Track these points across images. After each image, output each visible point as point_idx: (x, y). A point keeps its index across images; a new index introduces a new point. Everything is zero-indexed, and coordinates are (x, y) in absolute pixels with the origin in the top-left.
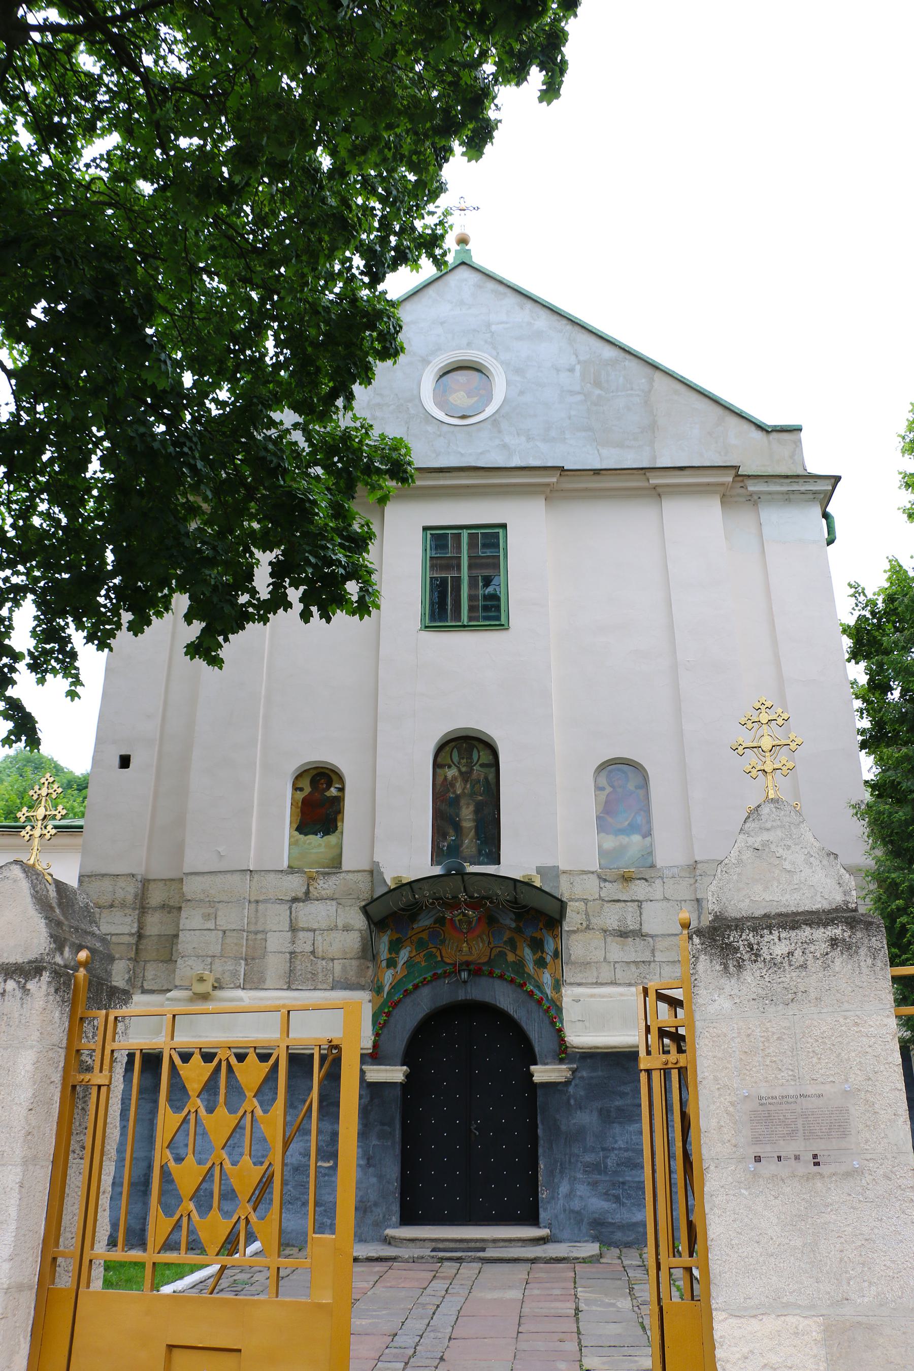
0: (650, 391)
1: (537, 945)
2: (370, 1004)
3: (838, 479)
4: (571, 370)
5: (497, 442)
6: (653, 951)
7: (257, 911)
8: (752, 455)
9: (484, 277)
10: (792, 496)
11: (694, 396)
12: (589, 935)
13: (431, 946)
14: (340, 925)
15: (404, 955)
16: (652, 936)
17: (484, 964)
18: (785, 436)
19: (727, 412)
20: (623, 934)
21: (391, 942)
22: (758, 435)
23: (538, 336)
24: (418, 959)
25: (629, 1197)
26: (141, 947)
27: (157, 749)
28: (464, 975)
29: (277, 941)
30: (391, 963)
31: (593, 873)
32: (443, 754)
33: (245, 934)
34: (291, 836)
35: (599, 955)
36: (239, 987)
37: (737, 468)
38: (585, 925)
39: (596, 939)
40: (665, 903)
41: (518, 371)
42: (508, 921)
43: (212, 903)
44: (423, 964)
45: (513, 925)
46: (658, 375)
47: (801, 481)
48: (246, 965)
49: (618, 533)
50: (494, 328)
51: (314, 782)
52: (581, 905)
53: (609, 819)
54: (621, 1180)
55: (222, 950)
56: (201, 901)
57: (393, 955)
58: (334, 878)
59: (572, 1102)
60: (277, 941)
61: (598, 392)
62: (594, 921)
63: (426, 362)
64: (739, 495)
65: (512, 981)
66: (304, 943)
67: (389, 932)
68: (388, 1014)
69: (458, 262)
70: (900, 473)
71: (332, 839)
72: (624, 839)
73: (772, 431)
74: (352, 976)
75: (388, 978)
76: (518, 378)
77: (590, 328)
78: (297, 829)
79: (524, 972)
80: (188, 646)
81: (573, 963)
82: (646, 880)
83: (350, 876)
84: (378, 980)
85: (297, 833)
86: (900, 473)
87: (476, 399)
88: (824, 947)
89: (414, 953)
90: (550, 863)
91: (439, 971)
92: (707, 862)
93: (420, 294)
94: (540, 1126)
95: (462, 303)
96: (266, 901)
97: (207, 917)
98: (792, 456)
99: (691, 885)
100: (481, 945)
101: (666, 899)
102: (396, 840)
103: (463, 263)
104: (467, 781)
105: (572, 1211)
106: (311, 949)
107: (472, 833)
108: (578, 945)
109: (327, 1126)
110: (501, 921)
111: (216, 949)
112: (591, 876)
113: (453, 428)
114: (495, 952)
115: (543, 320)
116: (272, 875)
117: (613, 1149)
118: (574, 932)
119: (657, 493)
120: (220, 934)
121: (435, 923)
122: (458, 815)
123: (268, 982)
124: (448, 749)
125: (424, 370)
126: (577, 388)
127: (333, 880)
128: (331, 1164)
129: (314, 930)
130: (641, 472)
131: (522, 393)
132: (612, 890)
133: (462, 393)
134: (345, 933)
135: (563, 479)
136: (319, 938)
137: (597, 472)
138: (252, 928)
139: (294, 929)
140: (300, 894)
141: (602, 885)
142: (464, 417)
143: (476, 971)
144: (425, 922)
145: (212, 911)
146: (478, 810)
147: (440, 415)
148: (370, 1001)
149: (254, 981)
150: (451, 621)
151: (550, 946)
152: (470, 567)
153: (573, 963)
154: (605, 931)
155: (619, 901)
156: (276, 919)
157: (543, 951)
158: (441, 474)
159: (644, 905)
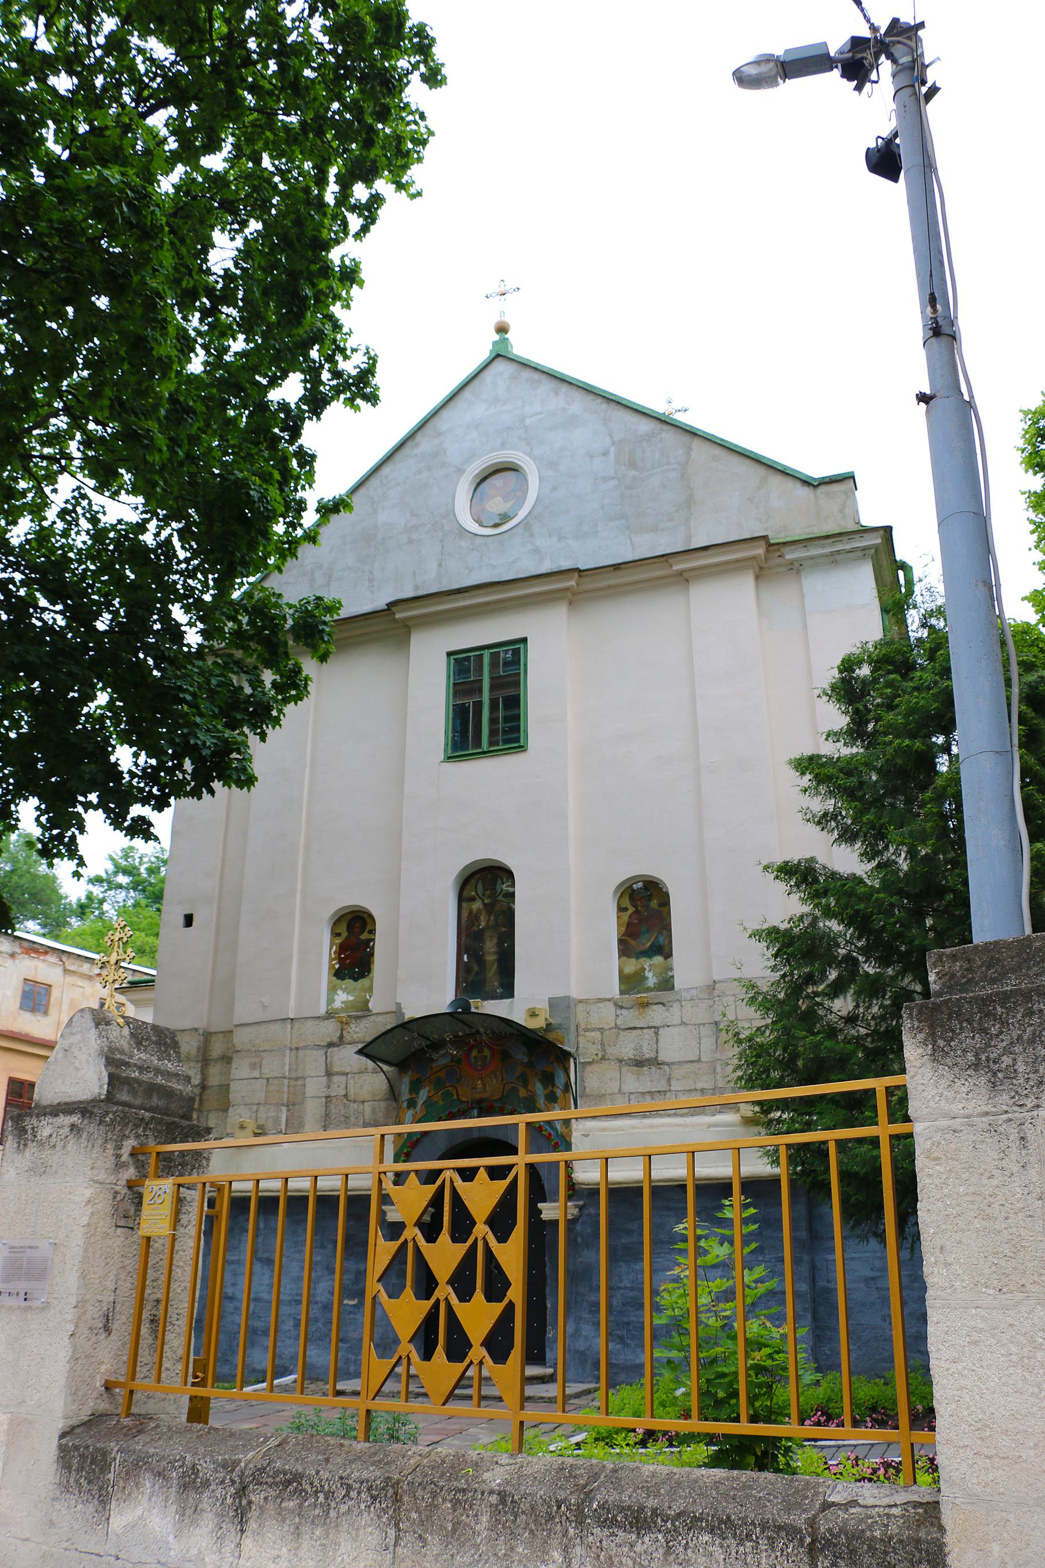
0: (687, 463)
1: (548, 1079)
4: (605, 454)
6: (669, 1080)
8: (789, 516)
9: (520, 366)
10: (837, 557)
11: (734, 459)
12: (604, 1065)
15: (423, 1095)
16: (668, 1064)
18: (835, 487)
19: (771, 471)
20: (639, 1063)
21: (411, 1083)
22: (804, 492)
24: (436, 1099)
25: (633, 1338)
26: (204, 1097)
27: (216, 905)
29: (315, 1087)
31: (609, 1000)
32: (468, 887)
33: (286, 1081)
34: (330, 982)
35: (614, 1087)
36: (281, 1132)
37: (765, 538)
38: (600, 1056)
41: (552, 465)
43: (258, 1053)
44: (441, 1103)
45: (526, 1060)
46: (696, 443)
47: (845, 538)
48: (288, 1110)
49: (642, 631)
50: (528, 421)
51: (350, 927)
52: (596, 1035)
53: (632, 942)
54: (626, 1320)
55: (266, 1097)
56: (248, 1051)
58: (364, 1021)
59: (579, 1240)
60: (315, 1087)
61: (633, 473)
62: (609, 1050)
63: (460, 471)
64: (779, 565)
67: (410, 1073)
69: (493, 355)
70: (1023, 493)
71: (364, 982)
73: (819, 485)
74: (380, 1115)
77: (629, 405)
80: (509, 874)
81: (588, 1096)
83: (379, 1018)
86: (1023, 493)
87: (512, 502)
88: (66, 1130)
89: (433, 1093)
91: (455, 1110)
92: (725, 981)
93: (456, 399)
94: (548, 1264)
95: (496, 400)
96: (305, 1048)
98: (841, 511)
99: (710, 1007)
101: (683, 1023)
102: (420, 979)
103: (498, 356)
105: (577, 1351)
106: (344, 1093)
107: (495, 967)
108: (594, 1078)
109: (352, 1266)
111: (260, 1097)
112: (608, 1003)
113: (485, 539)
115: (578, 403)
116: (310, 1022)
117: (619, 1288)
118: (590, 1063)
119: (684, 579)
120: (264, 1081)
122: (481, 949)
124: (473, 881)
125: (458, 481)
127: (364, 1024)
128: (355, 1302)
129: (347, 1074)
130: (662, 559)
131: (554, 489)
132: (629, 1017)
133: (499, 498)
135: (584, 580)
136: (351, 1082)
137: (616, 567)
138: (293, 1075)
139: (329, 1074)
140: (335, 1040)
141: (618, 1012)
142: (496, 526)
145: (257, 1060)
146: (500, 944)
150: (473, 748)
151: (560, 1081)
152: (493, 688)
153: (588, 1096)
154: (621, 1061)
155: (635, 1028)
156: (314, 1064)
157: (553, 1085)
158: (459, 596)
159: (661, 1031)
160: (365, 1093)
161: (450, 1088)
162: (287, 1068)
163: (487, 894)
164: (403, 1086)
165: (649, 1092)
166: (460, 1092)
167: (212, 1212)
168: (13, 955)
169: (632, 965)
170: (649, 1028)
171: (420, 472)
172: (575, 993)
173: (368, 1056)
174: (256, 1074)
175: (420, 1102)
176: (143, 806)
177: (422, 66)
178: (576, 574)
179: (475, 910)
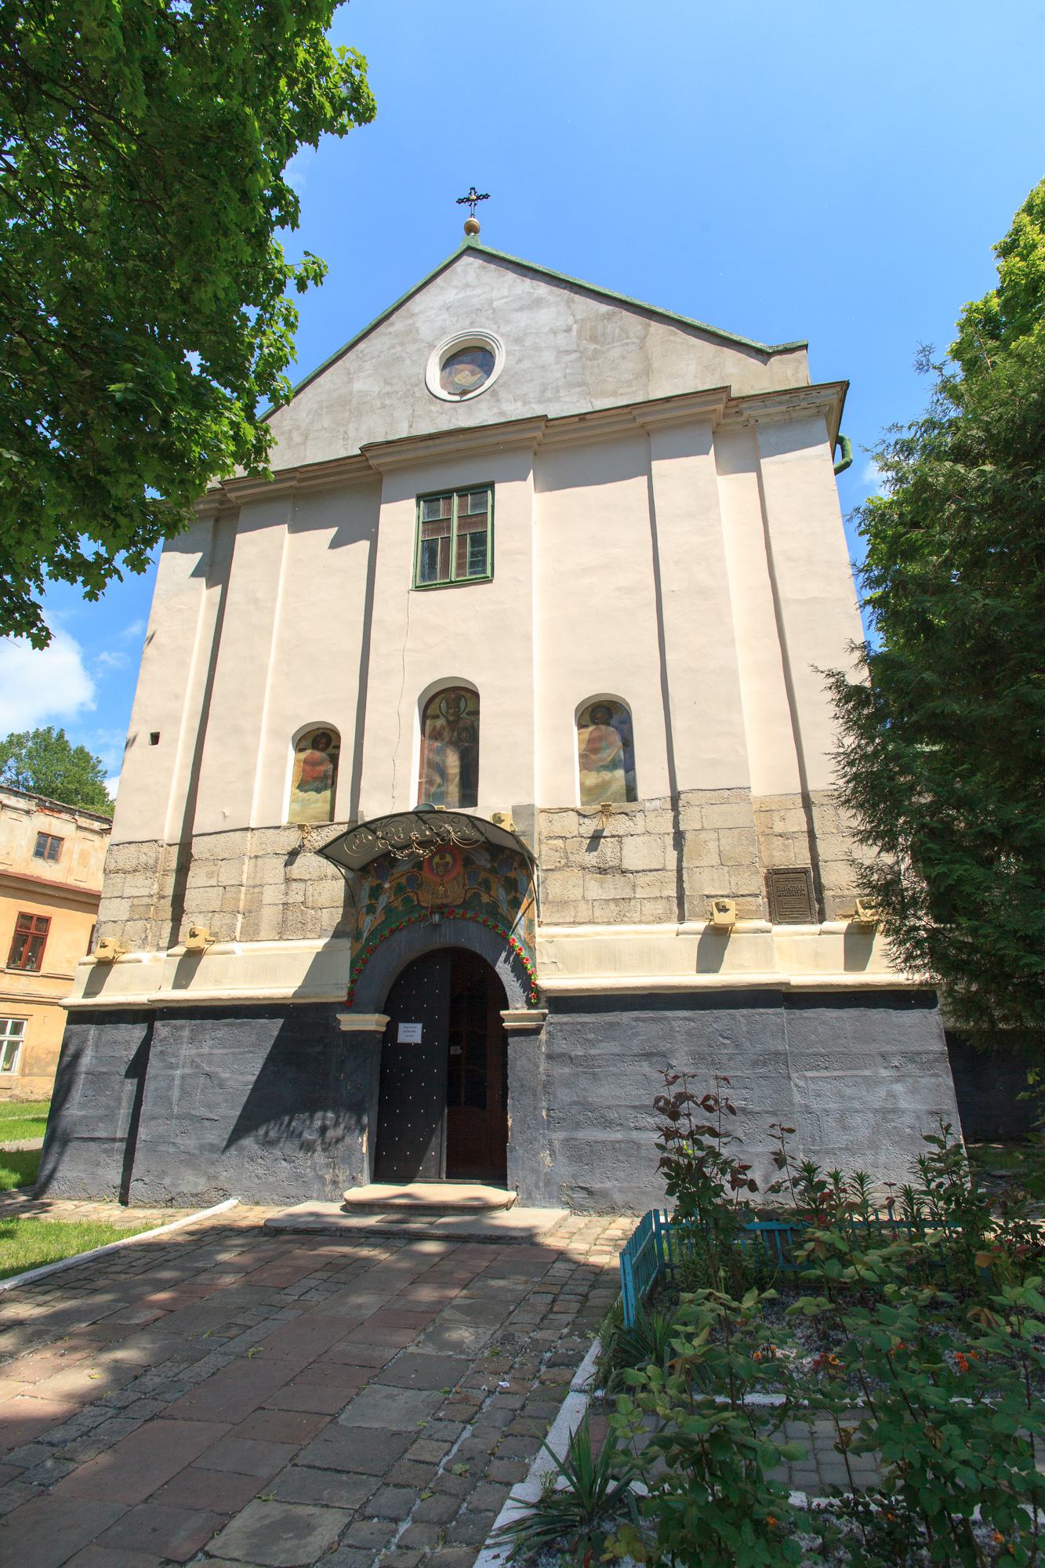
3: (845, 385)
4: (568, 330)
5: (495, 410)
12: (567, 873)
15: (383, 900)
21: (371, 889)
23: (538, 303)
24: (396, 904)
28: (436, 918)
30: (371, 909)
32: (432, 706)
34: (293, 794)
40: (646, 837)
41: (518, 341)
45: (489, 866)
50: (495, 304)
60: (272, 895)
61: (594, 346)
62: (572, 858)
66: (296, 895)
68: (365, 962)
72: (606, 775)
75: (368, 923)
76: (517, 348)
80: (475, 695)
90: (525, 801)
97: (210, 875)
111: (216, 906)
122: (444, 762)
124: (437, 700)
126: (574, 347)
131: (520, 361)
147: (443, 394)
149: (251, 934)
152: (460, 527)
160: (323, 900)
162: (245, 876)
163: (452, 714)
167: (14, 1038)
168: (28, 812)
169: (593, 779)
171: (393, 347)
172: (540, 803)
173: (327, 857)
175: (380, 907)
178: (543, 424)
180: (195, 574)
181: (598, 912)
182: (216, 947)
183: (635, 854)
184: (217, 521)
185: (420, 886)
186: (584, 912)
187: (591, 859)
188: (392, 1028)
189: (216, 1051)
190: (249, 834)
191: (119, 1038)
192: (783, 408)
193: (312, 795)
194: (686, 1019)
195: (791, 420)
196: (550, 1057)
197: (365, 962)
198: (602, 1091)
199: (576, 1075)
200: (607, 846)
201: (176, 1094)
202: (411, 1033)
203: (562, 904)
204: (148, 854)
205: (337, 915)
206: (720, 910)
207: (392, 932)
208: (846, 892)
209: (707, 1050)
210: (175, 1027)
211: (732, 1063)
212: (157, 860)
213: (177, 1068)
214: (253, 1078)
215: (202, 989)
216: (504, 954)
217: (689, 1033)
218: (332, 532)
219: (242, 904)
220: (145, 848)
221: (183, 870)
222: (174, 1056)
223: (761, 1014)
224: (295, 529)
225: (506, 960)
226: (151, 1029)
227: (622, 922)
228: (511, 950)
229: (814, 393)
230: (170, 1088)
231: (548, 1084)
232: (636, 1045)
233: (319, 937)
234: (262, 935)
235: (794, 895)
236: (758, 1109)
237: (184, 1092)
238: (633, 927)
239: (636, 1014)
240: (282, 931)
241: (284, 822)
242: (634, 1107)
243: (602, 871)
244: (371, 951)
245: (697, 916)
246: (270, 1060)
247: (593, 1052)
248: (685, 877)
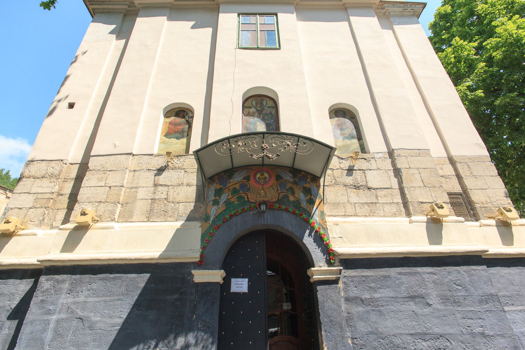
1: (307, 191)
2: (143, 24)
3: (424, 5)
7: (134, 176)
13: (241, 192)
14: (185, 183)
15: (224, 197)
17: (275, 202)
21: (216, 190)
24: (233, 200)
28: (263, 207)
30: (216, 203)
34: (161, 139)
39: (341, 190)
40: (378, 171)
42: (288, 177)
45: (292, 180)
56: (99, 170)
57: (217, 198)
62: (338, 180)
65: (293, 213)
66: (161, 194)
67: (215, 185)
68: (212, 235)
72: (348, 142)
75: (213, 211)
78: (165, 136)
79: (301, 207)
82: (365, 159)
84: (207, 213)
85: (165, 138)
89: (230, 196)
97: (101, 180)
100: (272, 191)
104: (260, 114)
110: (284, 178)
111: (103, 198)
114: (281, 195)
121: (244, 179)
123: (134, 217)
124: (250, 100)
129: (169, 186)
134: (188, 187)
143: (270, 206)
144: (238, 178)
148: (201, 227)
149: (127, 217)
160: (180, 197)
161: (243, 194)
164: (210, 193)
165: (366, 203)
166: (249, 197)
170: (360, 170)
174: (102, 184)
176: (45, 9)
177: (128, 175)
179: (251, 112)
180: (111, 33)
181: (358, 210)
182: (99, 225)
183: (374, 179)
184: (125, 15)
185: (249, 190)
186: (350, 210)
187: (349, 180)
188: (227, 281)
189: (90, 299)
190: (131, 157)
191: (6, 292)
192: (401, 9)
193: (174, 140)
194: (430, 273)
195: (403, 16)
196: (347, 300)
197: (212, 235)
198: (389, 323)
199: (367, 312)
200: (357, 175)
201: (49, 335)
202: (240, 285)
203: (336, 205)
204: (56, 168)
205: (191, 206)
206: (439, 208)
207: (231, 216)
208: (486, 205)
209: (449, 294)
210: (58, 281)
211: (466, 302)
212: (60, 171)
213: (54, 314)
214: (121, 321)
215: (85, 252)
216: (308, 232)
217: (434, 282)
218: (193, 23)
219: (121, 198)
220: (53, 164)
221: (79, 179)
222: (52, 303)
223: (474, 270)
224: (170, 19)
225: (310, 235)
226: (36, 283)
227: (373, 216)
228: (312, 228)
229: (413, 5)
230: (44, 330)
231: (349, 319)
232: (403, 291)
233: (177, 220)
234: (135, 218)
235: (464, 205)
236: (492, 333)
237: (57, 334)
238: (381, 219)
239: (399, 270)
240: (150, 216)
241: (155, 152)
242: (411, 334)
243: (357, 187)
244: (218, 228)
245: (417, 213)
246: (137, 305)
247: (376, 295)
248: (406, 192)
